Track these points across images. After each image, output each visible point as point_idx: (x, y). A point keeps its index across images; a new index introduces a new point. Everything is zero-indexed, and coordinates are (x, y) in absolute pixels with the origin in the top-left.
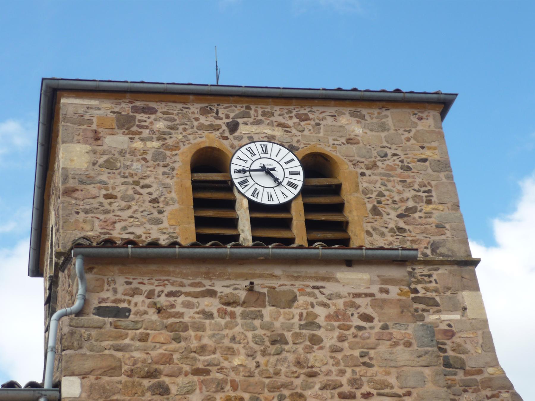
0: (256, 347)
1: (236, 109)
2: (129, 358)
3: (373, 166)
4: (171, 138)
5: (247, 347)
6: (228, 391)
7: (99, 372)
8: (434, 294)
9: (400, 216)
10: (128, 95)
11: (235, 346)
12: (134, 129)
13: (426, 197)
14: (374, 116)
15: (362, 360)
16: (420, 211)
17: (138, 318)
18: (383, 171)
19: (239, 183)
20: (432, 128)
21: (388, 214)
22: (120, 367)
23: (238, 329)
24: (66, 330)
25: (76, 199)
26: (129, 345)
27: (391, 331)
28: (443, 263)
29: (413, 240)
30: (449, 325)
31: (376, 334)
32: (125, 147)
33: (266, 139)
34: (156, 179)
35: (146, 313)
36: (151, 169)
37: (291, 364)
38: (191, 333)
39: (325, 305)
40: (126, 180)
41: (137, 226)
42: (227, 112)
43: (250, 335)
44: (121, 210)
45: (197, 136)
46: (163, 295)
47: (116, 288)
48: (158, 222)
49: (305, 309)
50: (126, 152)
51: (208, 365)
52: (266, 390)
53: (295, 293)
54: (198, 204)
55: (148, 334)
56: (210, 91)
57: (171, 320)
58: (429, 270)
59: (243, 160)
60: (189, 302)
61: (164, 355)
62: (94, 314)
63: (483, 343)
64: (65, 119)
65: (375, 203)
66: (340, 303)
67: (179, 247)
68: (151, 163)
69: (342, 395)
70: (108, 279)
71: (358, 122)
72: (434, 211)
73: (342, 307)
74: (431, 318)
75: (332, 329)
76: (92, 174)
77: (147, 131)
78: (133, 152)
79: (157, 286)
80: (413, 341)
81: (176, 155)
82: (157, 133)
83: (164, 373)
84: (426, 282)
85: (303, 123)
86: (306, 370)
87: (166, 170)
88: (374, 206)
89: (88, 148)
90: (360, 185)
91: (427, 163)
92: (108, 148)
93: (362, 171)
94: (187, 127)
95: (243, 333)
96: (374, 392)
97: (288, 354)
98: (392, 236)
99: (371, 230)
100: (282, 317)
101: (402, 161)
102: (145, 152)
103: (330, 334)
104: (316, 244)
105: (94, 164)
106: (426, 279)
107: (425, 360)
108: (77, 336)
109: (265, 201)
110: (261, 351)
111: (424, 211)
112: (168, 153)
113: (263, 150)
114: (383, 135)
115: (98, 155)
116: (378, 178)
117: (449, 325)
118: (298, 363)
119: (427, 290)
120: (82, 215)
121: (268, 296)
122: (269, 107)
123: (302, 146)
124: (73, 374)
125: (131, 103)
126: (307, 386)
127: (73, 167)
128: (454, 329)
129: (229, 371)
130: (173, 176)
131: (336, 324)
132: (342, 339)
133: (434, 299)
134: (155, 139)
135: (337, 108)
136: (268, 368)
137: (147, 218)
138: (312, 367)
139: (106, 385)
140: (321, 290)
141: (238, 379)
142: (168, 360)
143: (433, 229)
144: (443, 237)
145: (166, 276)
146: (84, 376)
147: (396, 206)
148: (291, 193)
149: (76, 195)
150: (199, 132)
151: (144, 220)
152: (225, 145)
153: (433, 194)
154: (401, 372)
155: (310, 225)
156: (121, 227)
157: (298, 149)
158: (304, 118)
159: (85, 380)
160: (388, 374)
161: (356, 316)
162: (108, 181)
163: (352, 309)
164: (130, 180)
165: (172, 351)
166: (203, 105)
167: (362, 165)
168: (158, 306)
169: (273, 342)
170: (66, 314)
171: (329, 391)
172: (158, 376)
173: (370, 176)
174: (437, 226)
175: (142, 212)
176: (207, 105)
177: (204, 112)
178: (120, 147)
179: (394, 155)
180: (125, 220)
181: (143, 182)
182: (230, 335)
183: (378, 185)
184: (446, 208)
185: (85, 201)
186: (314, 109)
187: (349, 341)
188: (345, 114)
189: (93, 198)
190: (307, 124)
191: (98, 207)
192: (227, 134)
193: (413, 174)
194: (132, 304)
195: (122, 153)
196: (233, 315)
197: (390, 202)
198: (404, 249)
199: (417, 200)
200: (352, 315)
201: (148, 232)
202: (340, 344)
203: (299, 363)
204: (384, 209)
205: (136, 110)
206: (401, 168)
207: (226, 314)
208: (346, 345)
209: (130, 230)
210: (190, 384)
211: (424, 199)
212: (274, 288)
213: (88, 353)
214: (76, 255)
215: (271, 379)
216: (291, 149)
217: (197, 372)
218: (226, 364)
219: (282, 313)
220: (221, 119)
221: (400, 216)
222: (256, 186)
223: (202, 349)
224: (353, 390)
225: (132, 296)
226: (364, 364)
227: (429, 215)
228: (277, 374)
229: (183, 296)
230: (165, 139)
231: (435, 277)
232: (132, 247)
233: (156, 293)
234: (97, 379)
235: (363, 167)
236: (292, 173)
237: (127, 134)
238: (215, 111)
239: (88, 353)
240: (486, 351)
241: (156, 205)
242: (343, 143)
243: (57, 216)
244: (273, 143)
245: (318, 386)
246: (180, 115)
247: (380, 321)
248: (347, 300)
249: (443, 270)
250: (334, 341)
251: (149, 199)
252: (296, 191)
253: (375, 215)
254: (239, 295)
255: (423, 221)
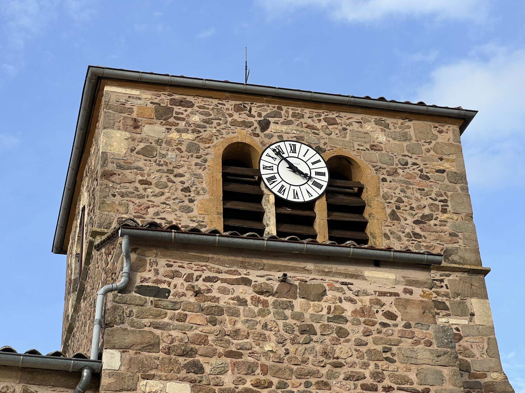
0: (287, 336)
1: (268, 108)
2: (167, 336)
3: (394, 173)
4: (205, 131)
5: (278, 335)
6: (258, 374)
7: (139, 347)
8: (445, 298)
9: (416, 222)
10: (168, 88)
11: (267, 333)
12: (172, 120)
13: (442, 206)
14: (397, 126)
15: (385, 355)
16: (436, 219)
17: (176, 299)
18: (403, 178)
19: (267, 179)
20: (451, 141)
21: (406, 220)
22: (159, 344)
23: (270, 317)
24: (109, 305)
25: (113, 182)
26: (168, 324)
27: (413, 329)
28: (454, 270)
29: (427, 246)
30: (457, 329)
31: (399, 331)
32: (162, 136)
33: (295, 139)
34: (188, 167)
35: (184, 295)
36: (185, 159)
37: (318, 354)
38: (226, 316)
39: (352, 301)
40: (161, 168)
41: (168, 212)
42: (259, 110)
43: (281, 323)
44: (155, 196)
45: (230, 131)
46: (201, 279)
47: (157, 269)
48: (189, 210)
49: (334, 303)
50: (162, 141)
51: (240, 349)
52: (294, 377)
53: (324, 287)
54: (227, 196)
55: (186, 315)
56: (246, 90)
57: (207, 304)
58: (441, 276)
59: (272, 158)
60: (225, 288)
61: (200, 335)
62: (135, 292)
63: (488, 349)
64: (108, 106)
65: (394, 208)
66: (366, 300)
67: (219, 236)
68: (185, 154)
69: (364, 387)
70: (150, 260)
71: (382, 130)
72: (448, 220)
73: (368, 304)
74: (441, 321)
75: (359, 323)
76: (131, 159)
77: (184, 123)
78: (169, 143)
79: (195, 270)
80: (434, 341)
81: (209, 147)
82: (192, 125)
83: (199, 353)
84: (438, 287)
85: (330, 127)
86: (332, 360)
87: (199, 161)
88: (393, 211)
89: (128, 135)
90: (381, 189)
91: (445, 174)
92: (146, 137)
93: (383, 176)
94: (221, 122)
95: (274, 321)
96: (395, 386)
97: (316, 344)
98: (408, 241)
99: (389, 234)
100: (311, 309)
101: (421, 171)
102: (180, 143)
103: (355, 328)
104: (348, 242)
105: (132, 150)
106: (438, 283)
107: (444, 359)
108: (119, 312)
109: (291, 198)
110: (291, 339)
111: (439, 219)
112: (202, 145)
113: (291, 149)
114: (405, 144)
115: (136, 143)
116: (398, 185)
117: (457, 329)
118: (325, 353)
119: (438, 294)
120: (118, 198)
121: (300, 289)
122: (300, 109)
123: (329, 148)
124: (114, 348)
125: (169, 95)
126: (331, 375)
127: (113, 152)
128: (461, 333)
129: (260, 356)
130: (205, 168)
131: (362, 319)
132: (367, 334)
133: (444, 303)
134: (190, 131)
135: (363, 116)
136: (296, 356)
137: (179, 205)
138: (338, 358)
139: (144, 360)
140: (349, 286)
141: (269, 363)
142: (203, 341)
143: (447, 237)
144: (456, 245)
145: (204, 262)
146: (124, 349)
147: (414, 213)
148: (316, 193)
149: (113, 178)
150: (232, 127)
151: (175, 207)
152: (255, 142)
153: (449, 203)
154: (421, 369)
155: (332, 225)
156: (153, 212)
157: (325, 151)
158: (331, 122)
159: (124, 354)
160: (410, 370)
161: (381, 313)
162: (145, 168)
163: (376, 306)
164: (165, 168)
165: (208, 333)
166: (238, 102)
167: (384, 171)
168: (196, 289)
169: (302, 332)
170: (111, 290)
171: (352, 382)
172: (194, 356)
173: (390, 182)
174: (450, 234)
175: (174, 199)
176: (241, 102)
177: (238, 109)
178: (157, 137)
179: (414, 164)
180: (158, 206)
181: (176, 171)
182: (263, 322)
183: (398, 191)
184: (460, 218)
185: (122, 185)
186: (342, 114)
187: (373, 336)
188: (370, 121)
189: (129, 183)
190: (334, 128)
191: (134, 191)
192: (258, 131)
193: (431, 183)
194: (172, 286)
195: (159, 142)
196: (265, 303)
197: (408, 208)
198: (430, 254)
199: (434, 209)
200: (377, 312)
201: (179, 219)
202: (364, 339)
203: (325, 353)
204: (402, 215)
205: (174, 102)
206: (420, 177)
207: (259, 302)
208: (370, 339)
209: (162, 215)
210: (223, 365)
211: (440, 208)
212: (306, 281)
213: (129, 328)
214: (122, 235)
215: (299, 367)
216: (319, 150)
217: (230, 354)
218: (257, 349)
219: (311, 305)
220: (254, 117)
221: (416, 222)
222: (283, 183)
223: (236, 333)
224: (375, 383)
225: (172, 278)
226: (387, 359)
227: (444, 223)
228: (305, 362)
229: (219, 281)
230: (199, 132)
231: (446, 282)
232: (175, 232)
233: (195, 277)
234: (136, 353)
235: (385, 173)
236: (317, 174)
237: (164, 125)
238: (248, 109)
239: (129, 328)
240: (490, 357)
241: (187, 194)
242: (367, 149)
243: (92, 196)
244: (302, 143)
245: (342, 376)
246: (215, 110)
247: (402, 320)
248: (373, 297)
249: (454, 276)
250: (360, 335)
251: (181, 188)
252: (321, 191)
253: (393, 219)
254: (272, 285)
255: (438, 228)
